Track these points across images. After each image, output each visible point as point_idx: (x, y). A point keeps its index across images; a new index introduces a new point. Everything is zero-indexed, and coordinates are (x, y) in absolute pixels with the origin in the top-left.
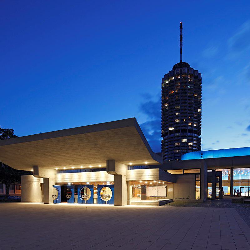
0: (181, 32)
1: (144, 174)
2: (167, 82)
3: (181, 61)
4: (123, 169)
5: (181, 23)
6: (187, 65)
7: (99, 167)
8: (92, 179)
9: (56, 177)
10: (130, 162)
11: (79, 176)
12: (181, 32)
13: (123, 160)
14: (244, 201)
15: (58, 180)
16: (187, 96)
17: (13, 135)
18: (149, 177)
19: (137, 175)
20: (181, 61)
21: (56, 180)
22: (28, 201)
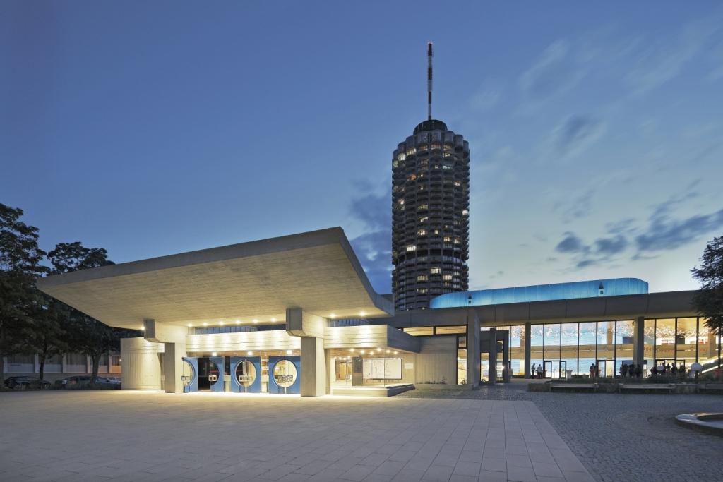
0: (430, 61)
2: (403, 158)
3: (430, 117)
5: (430, 45)
6: (440, 125)
12: (430, 61)
20: (430, 117)
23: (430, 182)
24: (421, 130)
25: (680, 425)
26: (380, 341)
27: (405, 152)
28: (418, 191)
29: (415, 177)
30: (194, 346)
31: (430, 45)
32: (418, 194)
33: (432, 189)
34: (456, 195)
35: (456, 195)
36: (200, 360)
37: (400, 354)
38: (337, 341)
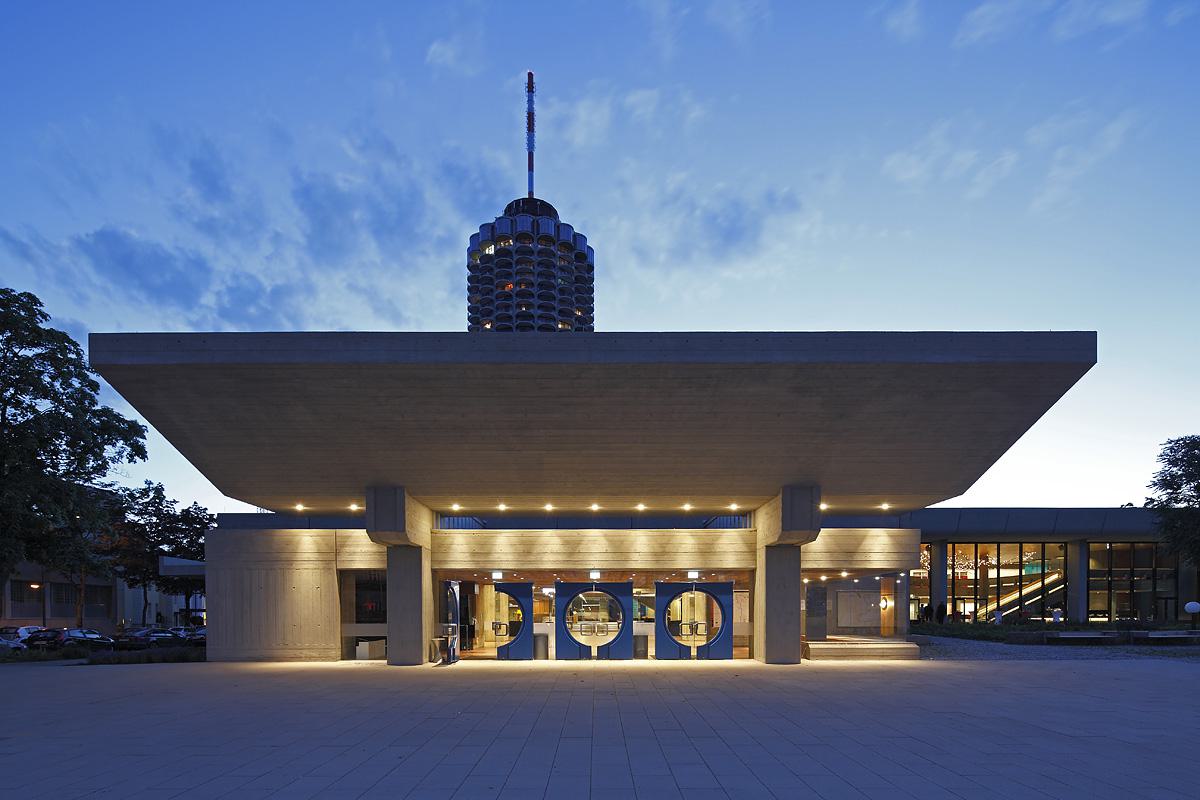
0: (530, 101)
1: (582, 548)
2: (491, 250)
3: (531, 193)
4: (422, 528)
5: (530, 75)
6: (548, 210)
7: (684, 511)
8: (874, 557)
9: (440, 545)
10: (640, 502)
11: (566, 543)
12: (530, 101)
13: (432, 488)
14: (1048, 638)
15: (452, 557)
16: (554, 308)
17: (44, 325)
18: (510, 557)
19: (324, 549)
20: (531, 193)
21: (441, 557)
22: (279, 653)
23: (536, 301)
24: (517, 212)
25: (533, 131)
26: (895, 556)
27: (494, 241)
28: (518, 311)
29: (511, 286)
30: (874, 557)
31: (530, 75)
32: (518, 316)
33: (540, 312)
34: (560, 312)
35: (560, 312)
36: (111, 587)
37: (587, 572)
38: (818, 556)
